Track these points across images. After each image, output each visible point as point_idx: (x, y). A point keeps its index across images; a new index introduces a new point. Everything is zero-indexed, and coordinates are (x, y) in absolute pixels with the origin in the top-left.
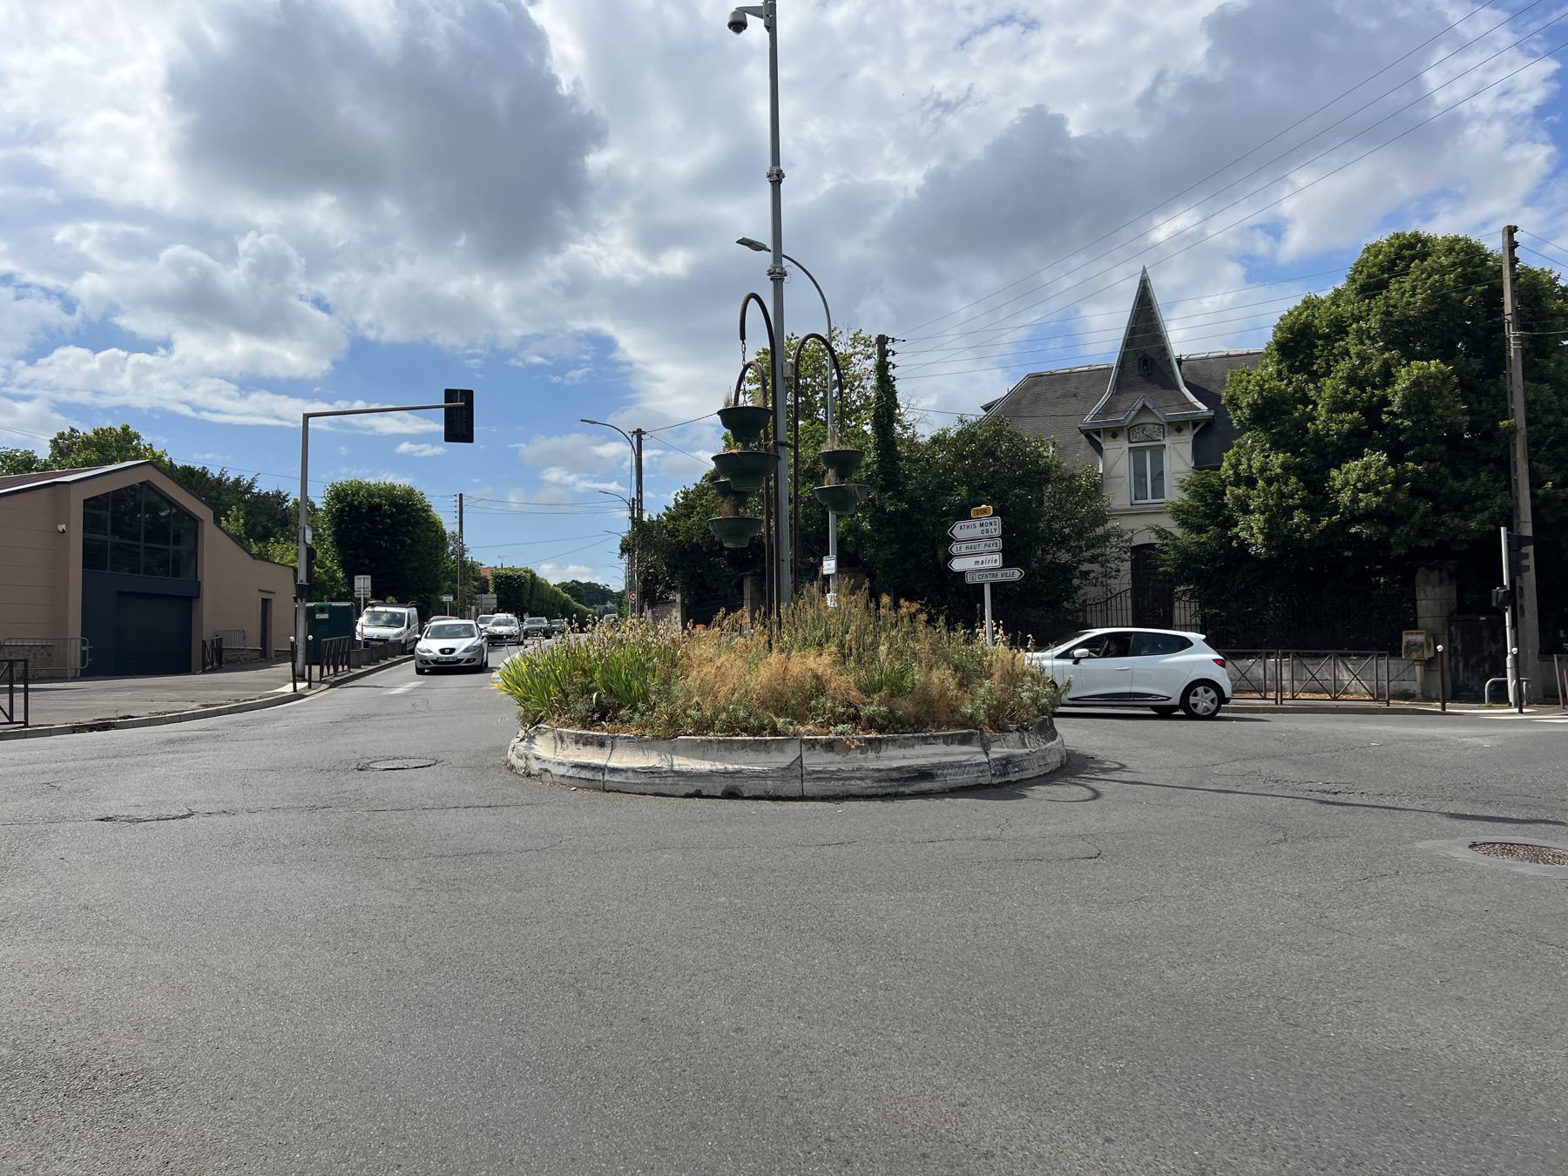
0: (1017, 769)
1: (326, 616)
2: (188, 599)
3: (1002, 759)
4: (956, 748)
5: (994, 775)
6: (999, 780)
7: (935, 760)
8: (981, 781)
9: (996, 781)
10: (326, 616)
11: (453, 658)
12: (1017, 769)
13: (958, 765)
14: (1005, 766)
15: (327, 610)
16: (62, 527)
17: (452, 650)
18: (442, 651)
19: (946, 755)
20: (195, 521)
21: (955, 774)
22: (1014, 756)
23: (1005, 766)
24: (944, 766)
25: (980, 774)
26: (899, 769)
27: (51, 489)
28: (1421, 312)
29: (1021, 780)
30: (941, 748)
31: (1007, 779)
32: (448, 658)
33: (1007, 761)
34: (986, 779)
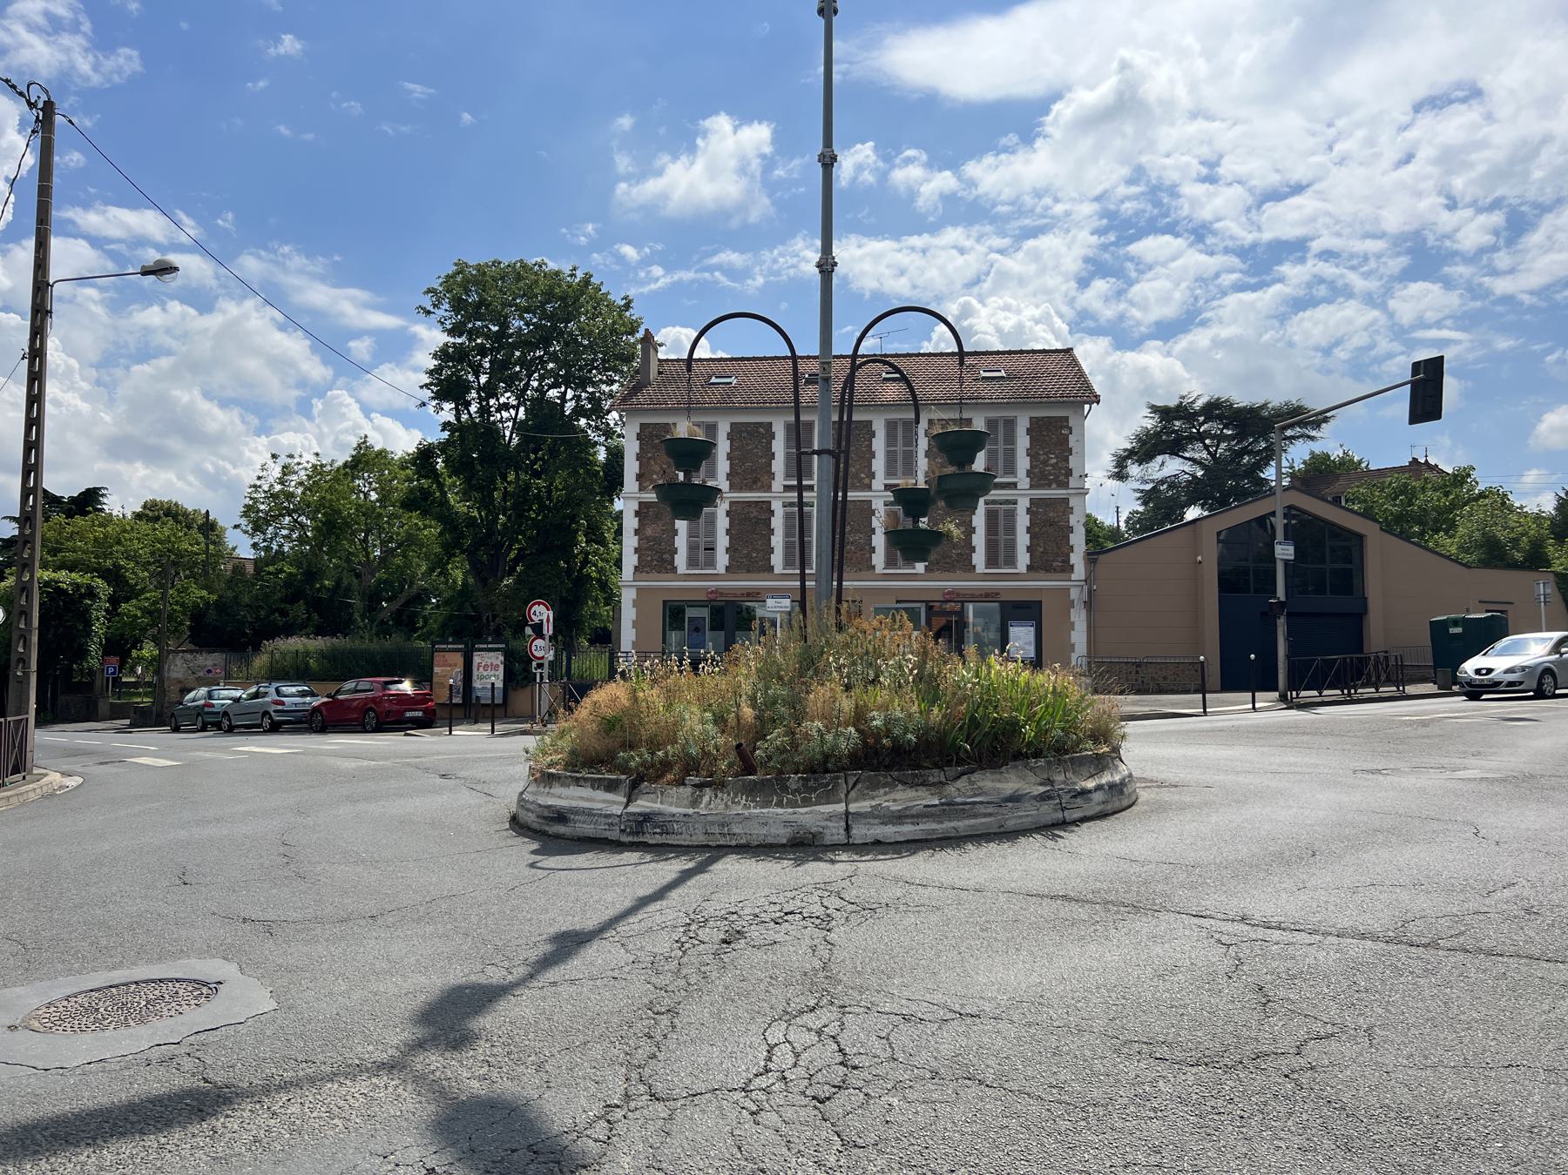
0: (658, 830)
1: (1459, 630)
2: (1356, 618)
3: (640, 814)
4: (601, 795)
5: (622, 831)
6: (630, 839)
7: (574, 804)
8: (608, 834)
9: (625, 839)
10: (1459, 630)
11: (1489, 680)
12: (658, 830)
13: (589, 813)
14: (640, 823)
15: (1460, 624)
16: (1199, 558)
17: (1490, 671)
18: (1478, 672)
19: (588, 800)
20: (1360, 538)
21: (584, 822)
22: (660, 814)
23: (640, 823)
24: (576, 811)
25: (607, 827)
26: (550, 806)
27: (1192, 526)
28: (109, 81)
29: (662, 845)
30: (587, 792)
31: (642, 840)
32: (1483, 680)
33: (647, 817)
34: (614, 835)
